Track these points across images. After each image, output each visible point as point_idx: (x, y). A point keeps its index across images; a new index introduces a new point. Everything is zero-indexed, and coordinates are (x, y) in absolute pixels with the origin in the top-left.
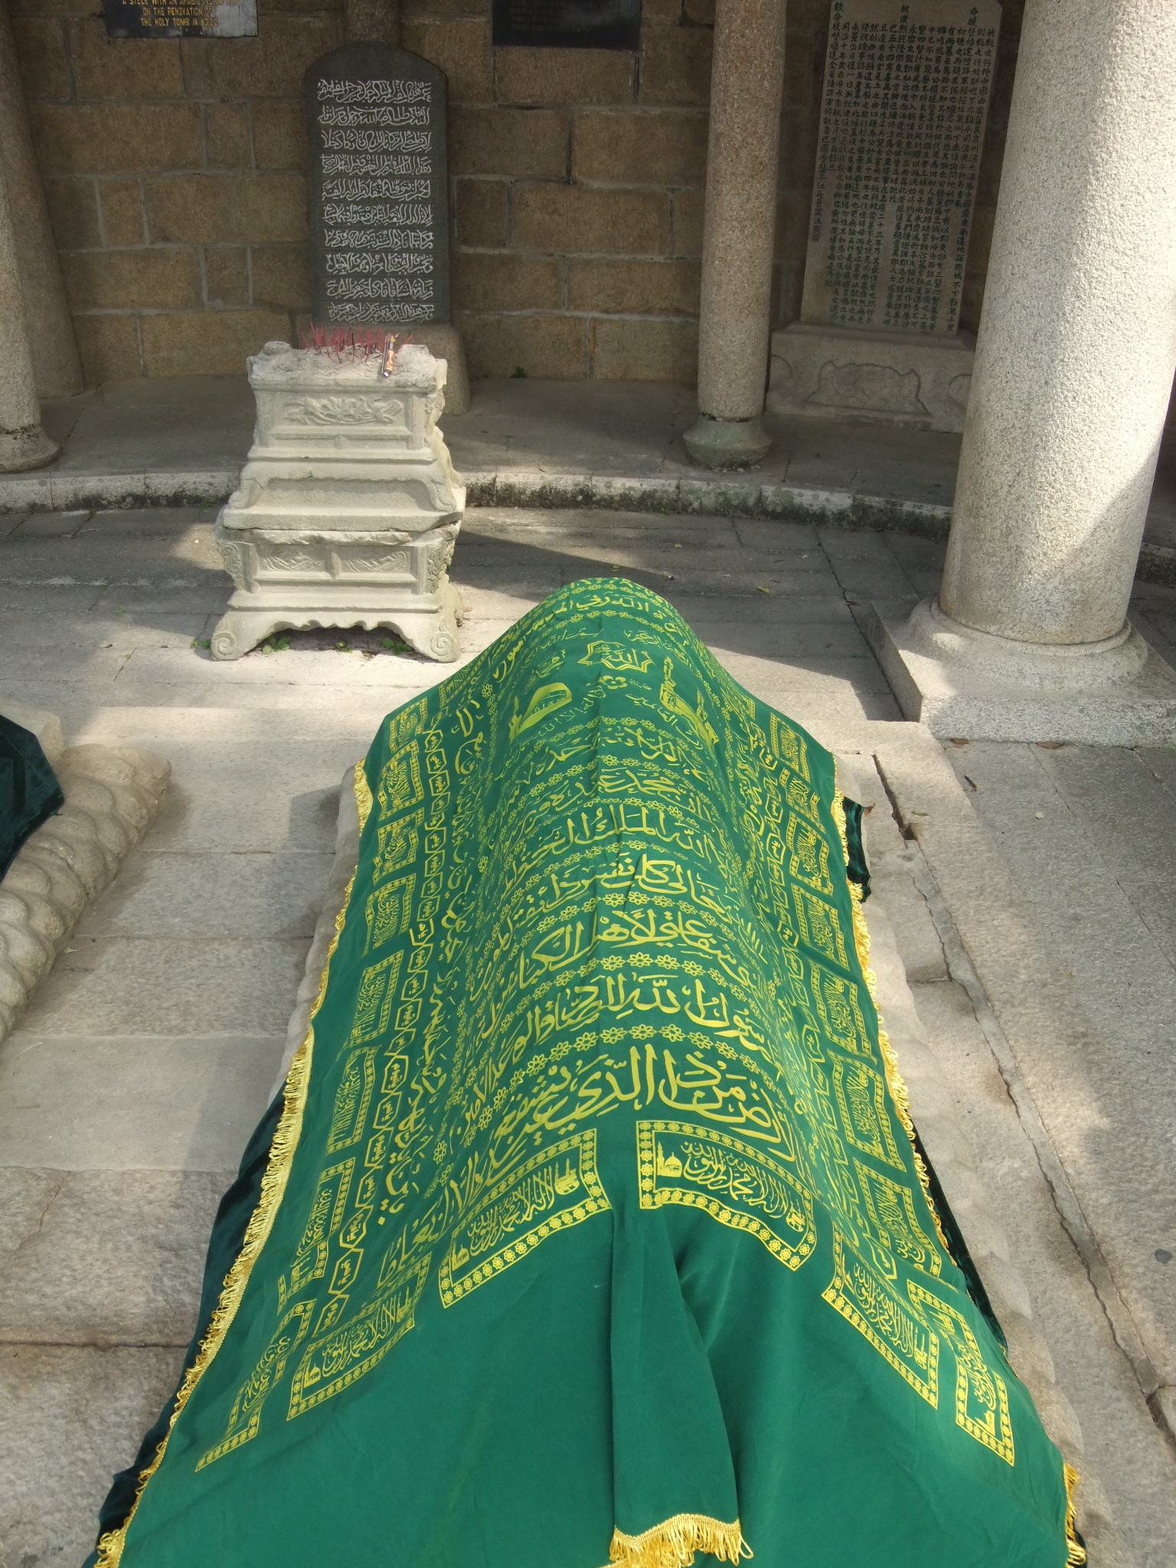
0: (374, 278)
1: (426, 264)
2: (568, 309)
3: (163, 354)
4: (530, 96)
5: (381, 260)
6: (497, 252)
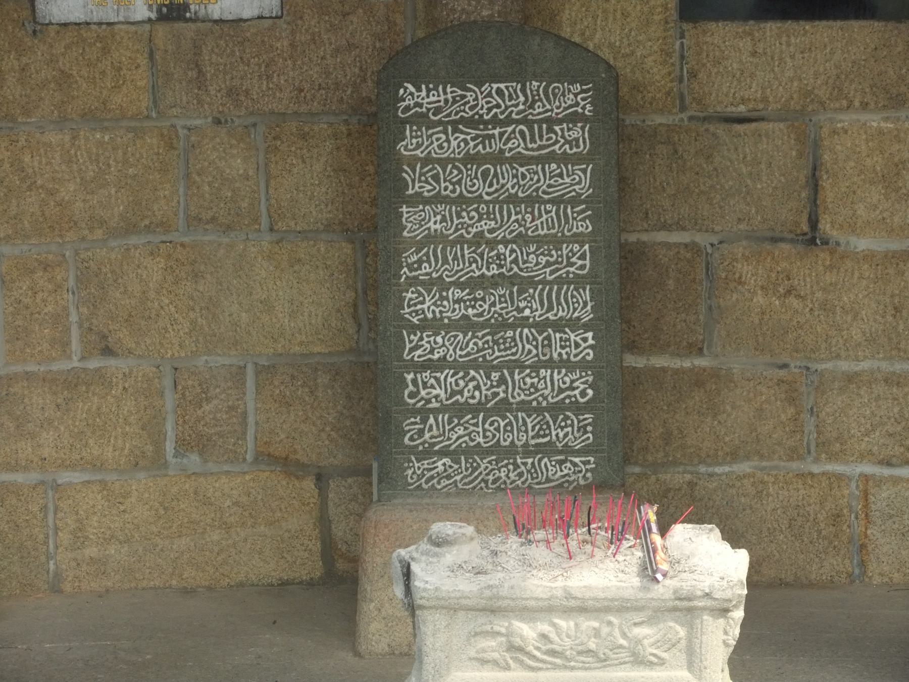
0: (489, 413)
1: (581, 387)
2: (817, 460)
3: (91, 551)
4: (743, 101)
5: (502, 381)
6: (687, 364)
